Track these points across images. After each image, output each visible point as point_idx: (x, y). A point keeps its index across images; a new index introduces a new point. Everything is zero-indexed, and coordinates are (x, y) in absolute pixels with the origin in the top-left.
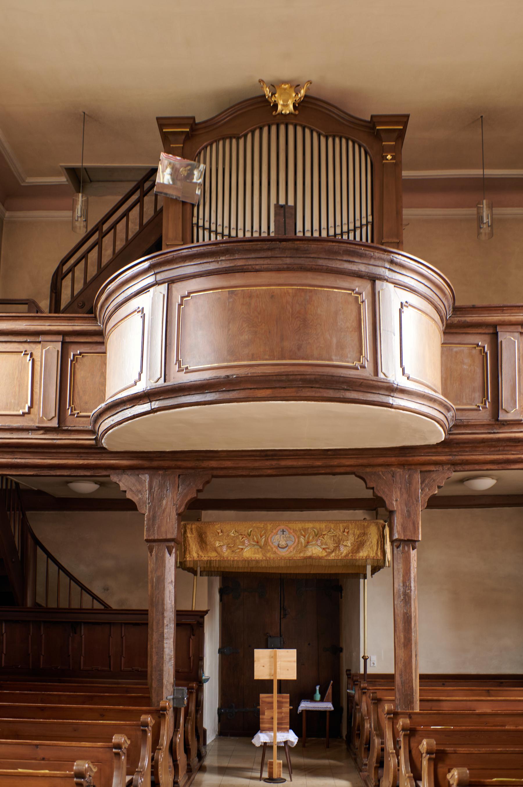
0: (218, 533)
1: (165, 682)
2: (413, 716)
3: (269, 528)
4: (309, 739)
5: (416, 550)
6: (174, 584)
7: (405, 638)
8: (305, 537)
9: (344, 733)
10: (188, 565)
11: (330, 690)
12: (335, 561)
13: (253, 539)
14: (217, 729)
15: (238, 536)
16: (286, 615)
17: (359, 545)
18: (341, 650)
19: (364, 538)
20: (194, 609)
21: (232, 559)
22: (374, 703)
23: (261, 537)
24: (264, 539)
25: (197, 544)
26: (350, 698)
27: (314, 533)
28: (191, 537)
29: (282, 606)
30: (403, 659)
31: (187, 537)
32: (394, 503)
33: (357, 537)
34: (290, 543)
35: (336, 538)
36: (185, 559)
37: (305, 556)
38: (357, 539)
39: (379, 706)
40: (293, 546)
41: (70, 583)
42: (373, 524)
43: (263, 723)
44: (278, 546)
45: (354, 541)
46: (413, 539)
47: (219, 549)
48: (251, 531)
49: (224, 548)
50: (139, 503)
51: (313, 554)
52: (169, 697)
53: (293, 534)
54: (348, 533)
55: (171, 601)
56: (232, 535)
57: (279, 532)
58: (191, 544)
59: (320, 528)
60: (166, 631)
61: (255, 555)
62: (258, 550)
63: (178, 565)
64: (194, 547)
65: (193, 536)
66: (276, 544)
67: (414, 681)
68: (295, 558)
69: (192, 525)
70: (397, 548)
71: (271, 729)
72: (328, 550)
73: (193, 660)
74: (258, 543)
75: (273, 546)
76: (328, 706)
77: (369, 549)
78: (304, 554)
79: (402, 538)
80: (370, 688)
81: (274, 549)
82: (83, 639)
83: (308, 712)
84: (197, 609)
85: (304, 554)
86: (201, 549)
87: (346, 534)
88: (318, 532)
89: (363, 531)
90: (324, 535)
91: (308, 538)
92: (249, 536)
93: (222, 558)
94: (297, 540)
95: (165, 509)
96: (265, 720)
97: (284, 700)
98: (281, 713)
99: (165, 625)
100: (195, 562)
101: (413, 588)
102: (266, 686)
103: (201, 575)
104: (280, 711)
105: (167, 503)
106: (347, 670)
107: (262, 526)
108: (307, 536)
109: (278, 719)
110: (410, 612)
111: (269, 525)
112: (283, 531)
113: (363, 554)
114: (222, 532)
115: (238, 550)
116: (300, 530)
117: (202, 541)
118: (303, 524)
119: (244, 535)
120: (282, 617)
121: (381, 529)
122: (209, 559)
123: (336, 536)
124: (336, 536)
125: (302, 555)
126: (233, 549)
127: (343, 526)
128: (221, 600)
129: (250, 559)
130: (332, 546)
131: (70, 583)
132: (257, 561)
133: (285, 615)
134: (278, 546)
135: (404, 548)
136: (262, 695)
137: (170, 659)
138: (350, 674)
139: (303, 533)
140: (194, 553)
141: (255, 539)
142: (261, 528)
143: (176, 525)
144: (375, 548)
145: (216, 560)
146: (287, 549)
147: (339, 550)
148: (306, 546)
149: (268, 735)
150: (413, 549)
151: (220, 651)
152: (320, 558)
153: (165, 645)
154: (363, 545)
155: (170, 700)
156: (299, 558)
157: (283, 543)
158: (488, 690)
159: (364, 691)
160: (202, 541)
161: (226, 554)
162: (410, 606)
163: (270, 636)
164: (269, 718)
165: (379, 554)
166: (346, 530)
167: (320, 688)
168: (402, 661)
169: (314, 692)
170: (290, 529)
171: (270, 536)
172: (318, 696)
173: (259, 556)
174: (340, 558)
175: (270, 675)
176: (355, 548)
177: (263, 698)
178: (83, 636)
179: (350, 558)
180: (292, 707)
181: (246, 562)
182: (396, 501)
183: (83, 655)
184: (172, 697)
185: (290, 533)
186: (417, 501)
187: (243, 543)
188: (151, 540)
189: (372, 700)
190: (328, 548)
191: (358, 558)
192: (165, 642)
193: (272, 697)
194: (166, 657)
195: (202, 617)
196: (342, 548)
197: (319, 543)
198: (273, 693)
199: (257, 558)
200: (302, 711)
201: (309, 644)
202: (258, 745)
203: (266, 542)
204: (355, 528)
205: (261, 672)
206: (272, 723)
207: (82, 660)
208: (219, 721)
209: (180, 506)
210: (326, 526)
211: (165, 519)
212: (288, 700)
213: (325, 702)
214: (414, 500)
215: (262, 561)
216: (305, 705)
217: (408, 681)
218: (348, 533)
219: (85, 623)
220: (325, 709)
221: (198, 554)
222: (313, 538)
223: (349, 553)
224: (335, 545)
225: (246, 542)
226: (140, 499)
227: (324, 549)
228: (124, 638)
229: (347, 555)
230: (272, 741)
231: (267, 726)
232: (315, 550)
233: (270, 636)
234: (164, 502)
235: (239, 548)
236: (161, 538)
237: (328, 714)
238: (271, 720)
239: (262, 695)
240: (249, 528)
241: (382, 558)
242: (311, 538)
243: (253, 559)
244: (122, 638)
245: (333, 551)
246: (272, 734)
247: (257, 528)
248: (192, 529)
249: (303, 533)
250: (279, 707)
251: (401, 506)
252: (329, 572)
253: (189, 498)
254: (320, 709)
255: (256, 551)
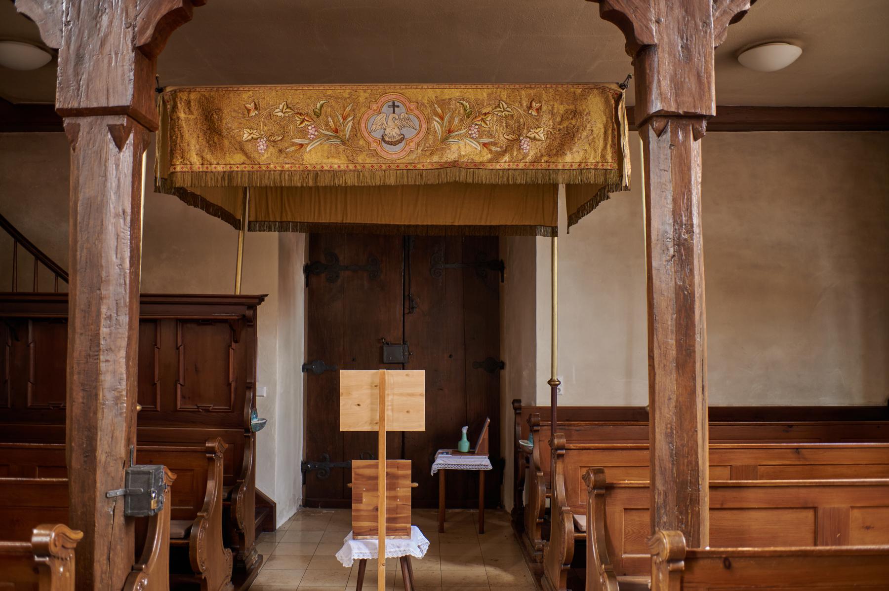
0: (249, 111)
1: (101, 456)
2: (736, 564)
3: (362, 100)
4: (450, 511)
5: (700, 140)
6: (129, 218)
7: (679, 346)
8: (442, 118)
9: (509, 504)
10: (179, 182)
11: (485, 435)
12: (511, 172)
13: (327, 124)
14: (300, 495)
15: (293, 116)
16: (413, 308)
17: (565, 138)
18: (502, 365)
19: (574, 122)
20: (238, 293)
21: (278, 168)
22: (597, 496)
23: (344, 119)
24: (350, 124)
25: (201, 135)
26: (523, 455)
27: (462, 110)
28: (187, 120)
29: (406, 294)
30: (674, 397)
31: (178, 118)
32: (654, 27)
33: (558, 119)
34: (409, 133)
35: (511, 122)
36: (172, 170)
37: (444, 160)
38: (560, 123)
39: (608, 500)
40: (417, 140)
41: (15, 247)
42: (595, 91)
43: (358, 519)
44: (383, 139)
45: (553, 129)
46: (698, 111)
47: (249, 147)
48: (322, 106)
49: (262, 145)
50: (45, 24)
51: (460, 156)
52: (112, 493)
53: (417, 112)
54: (539, 110)
55: (122, 259)
56: (280, 114)
57: (385, 108)
58: (186, 136)
59: (476, 100)
60: (104, 331)
61: (331, 160)
62: (336, 147)
63: (159, 183)
64: (193, 142)
65: (192, 117)
66: (378, 135)
67: (700, 450)
68: (420, 166)
69: (189, 92)
70: (659, 136)
71: (373, 531)
72: (494, 148)
73: (236, 389)
74: (337, 131)
75: (370, 140)
76: (482, 462)
77: (587, 147)
78: (441, 158)
79: (673, 109)
80: (572, 446)
81: (374, 145)
82: (32, 351)
83: (451, 474)
84: (244, 293)
85: (441, 158)
86: (210, 146)
87: (534, 113)
88: (472, 108)
89: (572, 107)
90: (485, 114)
91: (450, 122)
92: (318, 116)
93: (256, 167)
94: (424, 126)
95: (106, 36)
96: (362, 513)
97: (401, 472)
98: (395, 498)
99: (103, 316)
100: (196, 176)
101: (696, 230)
102: (365, 445)
103: (249, 230)
104: (392, 493)
105: (111, 22)
106: (515, 401)
107: (347, 95)
108: (446, 119)
109: (389, 510)
110: (692, 284)
111: (361, 93)
112: (394, 106)
113: (572, 158)
114: (256, 108)
115: (293, 148)
116: (432, 104)
117: (213, 130)
118: (439, 91)
119: (307, 114)
120: (407, 311)
121: (613, 101)
122: (227, 168)
123: (512, 116)
124: (512, 116)
125: (435, 159)
126: (281, 145)
127: (528, 95)
128: (307, 284)
129: (318, 167)
130: (503, 139)
131: (15, 247)
132: (335, 174)
133: (412, 308)
134: (383, 139)
135: (675, 134)
136: (355, 463)
137: (117, 399)
138: (520, 408)
139: (439, 111)
140: (194, 157)
141: (331, 124)
142: (345, 99)
143: (132, 74)
144: (601, 144)
145: (242, 171)
146: (402, 145)
147: (520, 148)
148: (445, 140)
149: (367, 545)
150: (695, 139)
151: (305, 368)
152: (477, 166)
153: (103, 366)
154: (573, 139)
155: (115, 499)
156: (429, 167)
157: (393, 132)
158: (797, 448)
159: (559, 452)
160: (213, 130)
161: (266, 156)
162: (692, 271)
163: (388, 344)
164: (371, 508)
165: (609, 157)
166: (534, 104)
167: (468, 431)
168: (673, 404)
169: (460, 438)
170: (410, 101)
171: (366, 116)
172: (465, 445)
173: (338, 162)
174: (521, 166)
175: (371, 423)
176: (556, 144)
177: (358, 468)
178: (32, 345)
179: (544, 166)
180: (416, 485)
181: (311, 176)
182: (658, 22)
183: (32, 380)
184: (120, 492)
185: (409, 110)
186: (706, 24)
187: (304, 133)
188: (71, 109)
189: (594, 488)
190: (495, 144)
191: (560, 167)
192: (102, 358)
193: (376, 466)
194: (106, 395)
195: (253, 307)
196: (526, 145)
197: (474, 130)
198: (377, 458)
199: (336, 167)
200: (439, 470)
201: (450, 356)
202: (347, 564)
203: (356, 131)
204: (554, 99)
205: (354, 416)
206: (376, 519)
207: (29, 389)
208: (304, 482)
209: (143, 31)
210: (489, 95)
211: (106, 61)
212: (409, 472)
213: (478, 454)
214: (698, 20)
215: (345, 172)
216: (443, 461)
217: (686, 449)
218: (539, 110)
219: (36, 320)
220: (477, 468)
221: (203, 158)
222: (461, 120)
223: (542, 155)
224: (510, 137)
225: (311, 130)
226: (46, 13)
227: (485, 145)
228: (181, 348)
229: (536, 160)
230: (376, 557)
231: (366, 524)
232: (465, 149)
233: (388, 344)
234: (105, 19)
235: (294, 144)
236: (95, 105)
237: (482, 477)
238: (374, 513)
239: (355, 463)
240: (318, 99)
241: (615, 166)
242: (456, 121)
243: (326, 168)
244: (178, 349)
245: (505, 151)
246: (375, 541)
247: (336, 98)
248: (189, 102)
249: (439, 111)
250: (391, 487)
251: (668, 35)
252: (488, 224)
253: (164, 11)
254: (468, 468)
255: (333, 150)
